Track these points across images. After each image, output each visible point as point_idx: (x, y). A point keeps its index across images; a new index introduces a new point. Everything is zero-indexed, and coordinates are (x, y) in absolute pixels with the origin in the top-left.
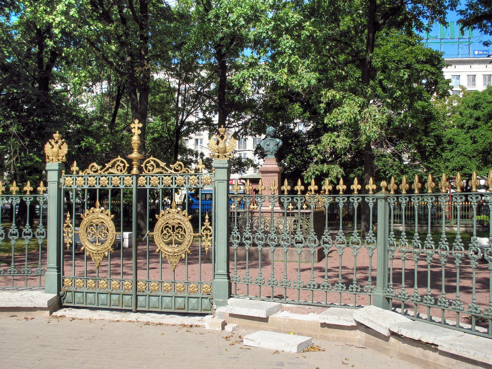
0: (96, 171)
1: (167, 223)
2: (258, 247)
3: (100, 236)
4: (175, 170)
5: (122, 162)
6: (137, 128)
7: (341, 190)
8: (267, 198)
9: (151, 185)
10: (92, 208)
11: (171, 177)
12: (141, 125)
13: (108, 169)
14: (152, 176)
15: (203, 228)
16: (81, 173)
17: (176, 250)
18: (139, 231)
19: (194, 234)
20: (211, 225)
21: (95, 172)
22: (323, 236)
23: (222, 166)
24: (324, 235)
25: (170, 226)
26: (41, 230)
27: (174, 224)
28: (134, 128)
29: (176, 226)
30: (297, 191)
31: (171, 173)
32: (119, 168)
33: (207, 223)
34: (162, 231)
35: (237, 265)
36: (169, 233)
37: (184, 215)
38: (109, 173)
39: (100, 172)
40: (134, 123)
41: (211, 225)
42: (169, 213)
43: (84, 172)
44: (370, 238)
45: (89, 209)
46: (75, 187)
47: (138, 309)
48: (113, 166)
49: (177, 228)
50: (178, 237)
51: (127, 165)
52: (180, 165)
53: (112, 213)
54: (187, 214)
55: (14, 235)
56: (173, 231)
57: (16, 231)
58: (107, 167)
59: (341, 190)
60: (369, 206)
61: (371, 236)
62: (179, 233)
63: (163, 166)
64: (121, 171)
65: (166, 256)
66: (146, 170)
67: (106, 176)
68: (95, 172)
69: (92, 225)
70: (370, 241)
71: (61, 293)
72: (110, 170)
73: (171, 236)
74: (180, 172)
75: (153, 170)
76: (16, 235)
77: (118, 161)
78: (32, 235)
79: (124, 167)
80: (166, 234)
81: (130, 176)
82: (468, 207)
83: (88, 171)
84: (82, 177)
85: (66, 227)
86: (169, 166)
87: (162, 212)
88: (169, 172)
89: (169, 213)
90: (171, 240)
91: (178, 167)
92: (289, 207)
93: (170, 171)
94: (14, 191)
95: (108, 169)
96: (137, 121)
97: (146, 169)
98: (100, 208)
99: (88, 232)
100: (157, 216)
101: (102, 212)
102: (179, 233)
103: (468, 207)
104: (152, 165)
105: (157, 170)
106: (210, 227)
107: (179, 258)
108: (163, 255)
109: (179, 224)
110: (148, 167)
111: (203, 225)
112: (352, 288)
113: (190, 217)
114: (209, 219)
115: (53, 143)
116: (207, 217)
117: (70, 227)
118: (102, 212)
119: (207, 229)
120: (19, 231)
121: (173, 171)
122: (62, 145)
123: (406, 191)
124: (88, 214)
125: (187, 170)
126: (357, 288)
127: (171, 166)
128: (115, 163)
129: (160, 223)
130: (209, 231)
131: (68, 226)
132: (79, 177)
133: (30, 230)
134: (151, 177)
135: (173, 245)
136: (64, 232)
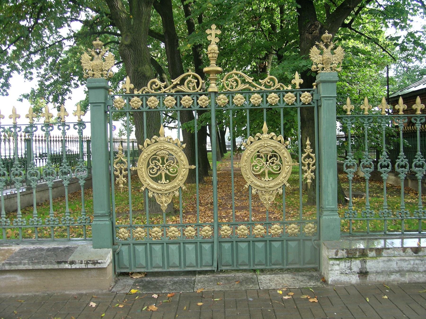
0: (160, 89)
1: (155, 154)
2: (348, 176)
3: (168, 172)
5: (196, 78)
6: (213, 35)
8: (72, 125)
10: (258, 134)
12: (219, 32)
16: (136, 92)
17: (168, 187)
20: (313, 152)
21: (156, 90)
24: (416, 158)
26: (402, 161)
27: (163, 155)
28: (211, 34)
30: (416, 110)
31: (261, 89)
32: (191, 85)
34: (148, 164)
36: (157, 166)
37: (280, 141)
39: (163, 90)
40: (211, 29)
43: (141, 90)
44: (17, 170)
45: (150, 137)
49: (270, 158)
50: (272, 169)
52: (272, 79)
55: (402, 167)
56: (163, 163)
57: (389, 161)
58: (175, 83)
61: (419, 158)
62: (273, 163)
63: (251, 81)
67: (172, 95)
72: (179, 88)
73: (159, 169)
74: (272, 88)
76: (387, 167)
77: (189, 76)
79: (198, 84)
80: (153, 168)
83: (148, 88)
85: (306, 157)
88: (258, 89)
89: (156, 142)
90: (264, 172)
95: (175, 87)
96: (214, 27)
98: (269, 133)
99: (150, 166)
101: (272, 138)
102: (169, 166)
107: (275, 193)
108: (254, 192)
109: (273, 151)
111: (303, 152)
115: (322, 46)
116: (308, 142)
118: (272, 138)
121: (263, 88)
124: (148, 145)
127: (260, 81)
131: (309, 157)
135: (267, 178)
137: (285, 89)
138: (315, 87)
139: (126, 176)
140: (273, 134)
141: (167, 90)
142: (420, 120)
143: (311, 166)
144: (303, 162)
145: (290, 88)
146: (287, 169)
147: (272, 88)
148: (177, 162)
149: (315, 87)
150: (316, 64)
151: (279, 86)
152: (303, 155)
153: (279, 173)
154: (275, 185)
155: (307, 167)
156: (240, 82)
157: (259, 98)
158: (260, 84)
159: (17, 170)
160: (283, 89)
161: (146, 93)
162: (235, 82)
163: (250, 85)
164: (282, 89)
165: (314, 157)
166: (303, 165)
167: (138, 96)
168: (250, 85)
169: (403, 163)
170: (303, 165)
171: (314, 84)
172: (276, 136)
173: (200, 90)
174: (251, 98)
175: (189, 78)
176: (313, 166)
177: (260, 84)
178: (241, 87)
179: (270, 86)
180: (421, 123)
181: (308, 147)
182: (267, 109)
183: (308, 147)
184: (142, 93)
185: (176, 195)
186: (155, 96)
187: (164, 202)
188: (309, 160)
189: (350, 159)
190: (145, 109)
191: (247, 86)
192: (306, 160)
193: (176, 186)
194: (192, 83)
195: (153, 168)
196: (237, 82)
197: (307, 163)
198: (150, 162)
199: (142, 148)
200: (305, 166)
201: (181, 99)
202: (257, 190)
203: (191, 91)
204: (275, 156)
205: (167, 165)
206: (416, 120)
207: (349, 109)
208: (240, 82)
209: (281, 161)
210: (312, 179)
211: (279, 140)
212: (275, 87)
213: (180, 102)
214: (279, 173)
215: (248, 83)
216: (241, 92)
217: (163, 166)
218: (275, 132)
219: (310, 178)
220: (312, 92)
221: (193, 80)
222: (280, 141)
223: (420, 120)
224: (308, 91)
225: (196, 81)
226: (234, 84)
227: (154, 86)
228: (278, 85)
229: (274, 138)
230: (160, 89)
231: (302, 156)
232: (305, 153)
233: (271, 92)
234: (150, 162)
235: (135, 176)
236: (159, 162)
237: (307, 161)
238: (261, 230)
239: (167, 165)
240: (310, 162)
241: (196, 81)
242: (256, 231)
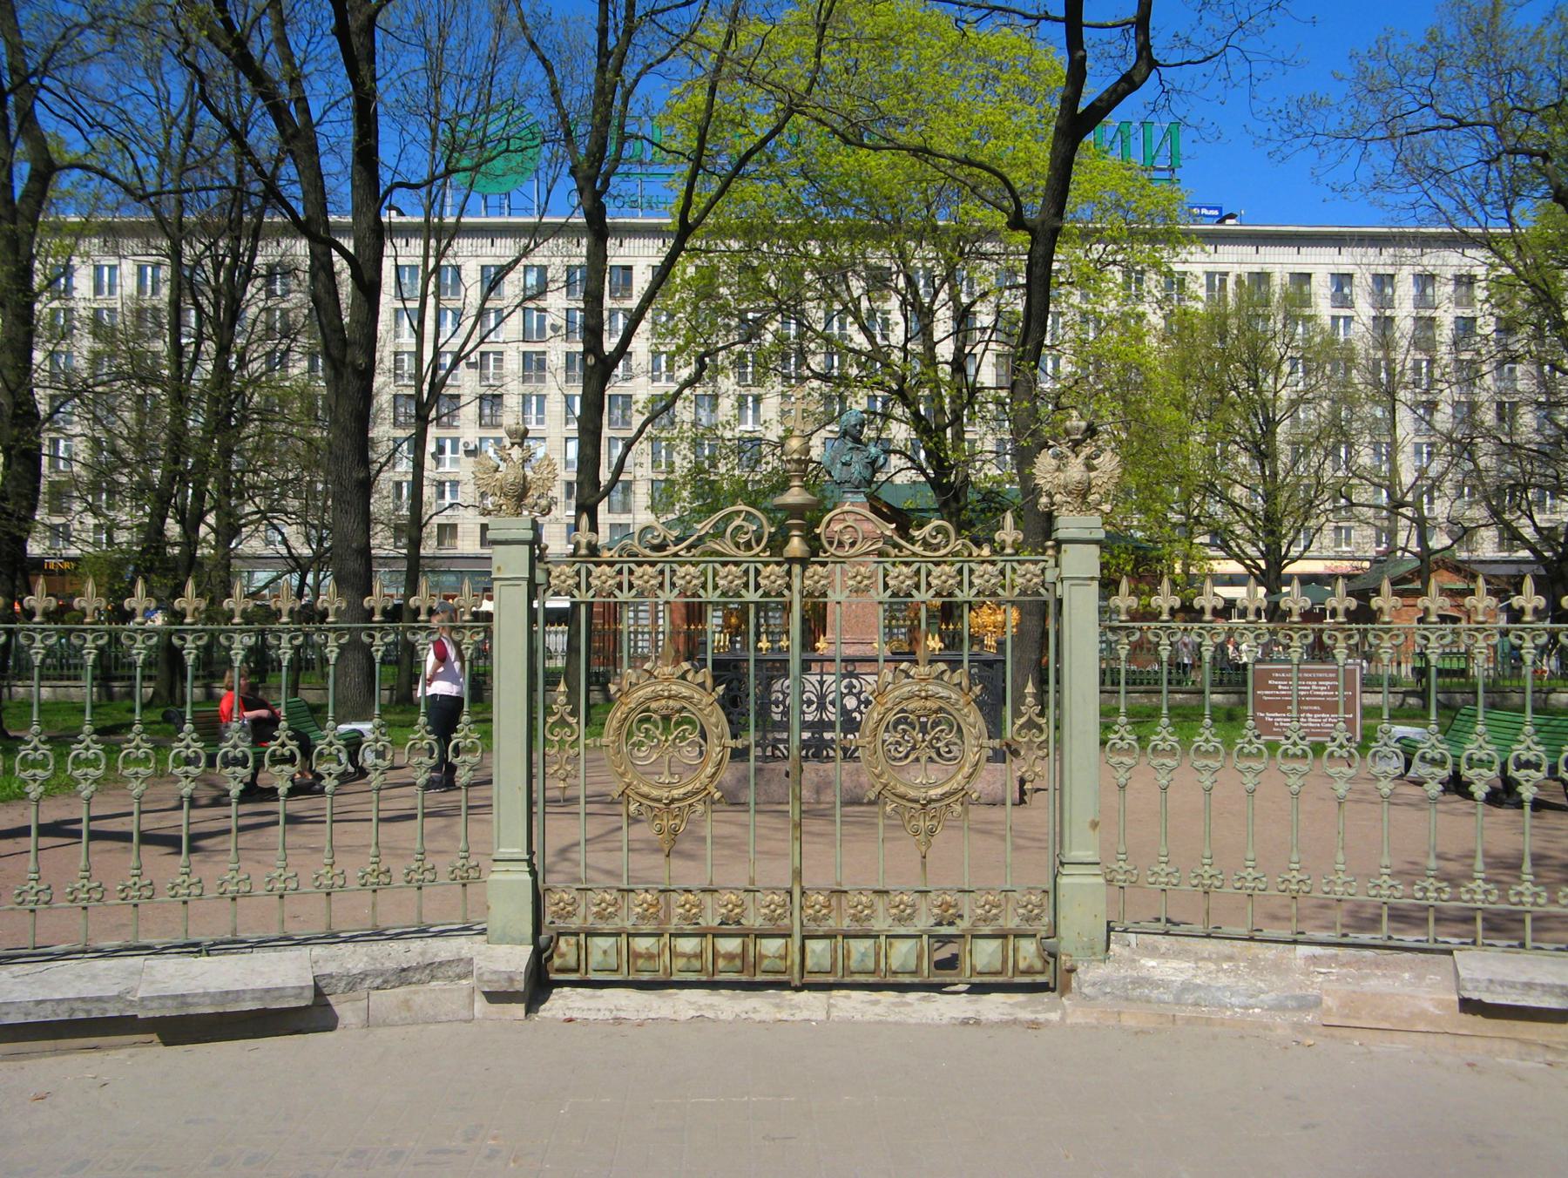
4: (926, 544)
9: (761, 592)
11: (915, 566)
14: (937, 564)
19: (732, 743)
22: (1154, 737)
23: (1086, 535)
31: (914, 554)
33: (1030, 706)
35: (238, 816)
37: (702, 685)
38: (703, 554)
46: (588, 597)
47: (809, 979)
48: (718, 533)
49: (678, 724)
51: (770, 529)
54: (709, 682)
59: (285, 612)
60: (182, 658)
62: (684, 739)
65: (643, 809)
69: (648, 719)
70: (1162, 746)
71: (543, 938)
74: (943, 552)
78: (1544, 768)
80: (641, 744)
81: (779, 564)
82: (170, 657)
84: (611, 564)
86: (907, 533)
94: (1166, 607)
103: (170, 657)
112: (1520, 894)
113: (721, 689)
114: (1035, 696)
116: (1030, 689)
117: (569, 725)
118: (683, 677)
119: (1030, 725)
120: (299, 747)
121: (918, 549)
123: (1301, 615)
126: (1535, 895)
128: (728, 518)
132: (598, 564)
133: (1443, 748)
134: (931, 566)
140: (686, 666)
142: (292, 638)
147: (943, 552)
148: (960, 729)
150: (1050, 495)
154: (686, 796)
159: (1122, 739)
169: (141, 754)
173: (764, 550)
175: (738, 522)
177: (912, 541)
180: (1536, 647)
181: (1029, 700)
182: (756, 603)
183: (1029, 700)
189: (1164, 733)
206: (1520, 638)
207: (190, 609)
211: (956, 681)
220: (1041, 565)
222: (702, 685)
223: (292, 638)
228: (956, 544)
229: (689, 677)
232: (1022, 715)
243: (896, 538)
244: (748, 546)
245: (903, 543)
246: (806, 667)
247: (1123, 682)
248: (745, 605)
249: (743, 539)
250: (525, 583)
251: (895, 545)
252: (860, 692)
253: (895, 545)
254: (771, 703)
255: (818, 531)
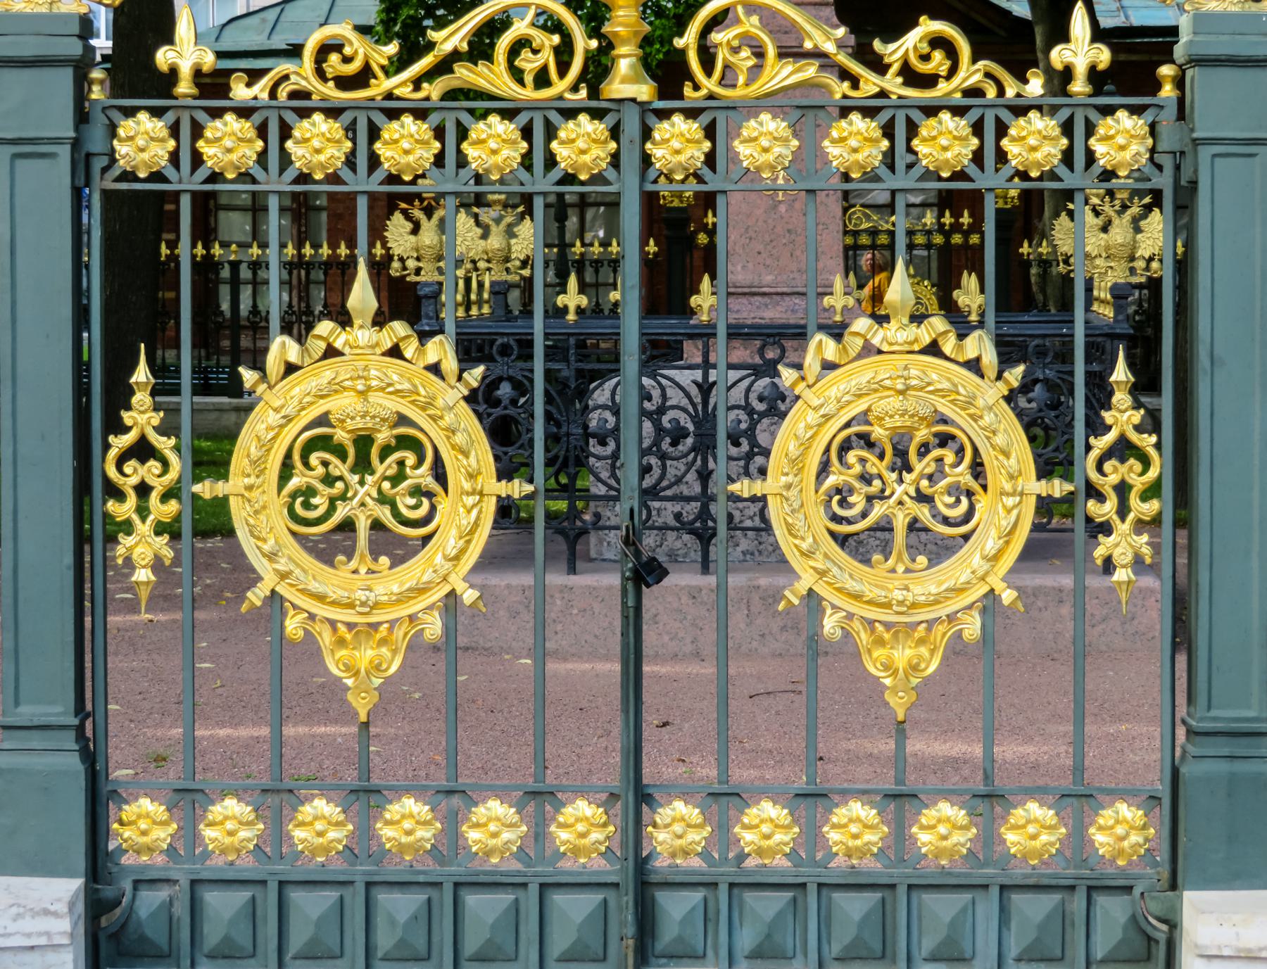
0: (363, 78)
3: (385, 514)
4: (911, 76)
7: (572, 309)
10: (325, 327)
13: (444, 67)
15: (1102, 443)
18: (440, 471)
21: (344, 83)
25: (341, 436)
29: (383, 436)
31: (883, 94)
32: (529, 63)
34: (286, 470)
37: (435, 369)
41: (1152, 423)
42: (331, 352)
48: (480, 49)
53: (1008, 352)
58: (448, 47)
59: (572, 309)
63: (830, 47)
64: (542, 79)
66: (709, 72)
68: (344, 83)
72: (464, 74)
74: (943, 87)
75: (756, 70)
87: (282, 348)
89: (331, 352)
91: (926, 58)
92: (561, 300)
93: (871, 83)
95: (444, 67)
97: (708, 61)
100: (248, 376)
104: (748, 40)
105: (780, 74)
106: (1147, 441)
109: (403, 420)
110: (722, 56)
111: (1096, 427)
121: (893, 83)
122: (1144, 216)
125: (988, 75)
129: (273, 418)
130: (1138, 467)
136: (115, 492)
137: (1010, 93)
138: (1168, 91)
139: (169, 529)
140: (399, 328)
141: (403, 84)
143: (154, 497)
144: (1094, 476)
145: (1035, 86)
146: (1009, 511)
149: (1168, 91)
151: (978, 77)
152: (111, 438)
153: (966, 537)
154: (402, 599)
155: (1111, 505)
156: (771, 51)
157: (873, 141)
158: (879, 67)
160: (1001, 92)
161: (294, 95)
162: (746, 52)
163: (822, 67)
164: (991, 93)
165: (1153, 453)
166: (1093, 492)
167: (244, 112)
168: (822, 67)
170: (1093, 492)
171: (1166, 70)
172: (414, 343)
173: (575, 88)
174: (916, 135)
176: (165, 497)
177: (879, 67)
178: (780, 74)
179: (929, 81)
181: (1121, 398)
182: (372, 197)
184: (273, 94)
185: (966, 635)
186: (333, 112)
187: (362, 669)
188: (1123, 469)
190: (187, 182)
191: (810, 70)
192: (127, 469)
193: (421, 590)
194: (535, 52)
195: (309, 492)
196: (760, 54)
197: (134, 480)
198: (296, 457)
199: (255, 384)
200: (1101, 498)
201: (463, 133)
202: (850, 616)
203: (528, 93)
204: (944, 440)
205: (386, 478)
208: (771, 51)
209: (978, 469)
210: (157, 565)
212: (956, 81)
213: (459, 151)
214: (966, 537)
215: (818, 54)
216: (773, 102)
217: (901, 481)
218: (413, 320)
219: (1129, 558)
221: (539, 37)
224: (1136, 110)
225: (556, 39)
226: (745, 59)
227: (334, 58)
228: (971, 73)
230: (363, 78)
231: (1088, 448)
232: (127, 430)
233: (931, 111)
234: (296, 457)
235: (213, 523)
236: (343, 458)
237: (1115, 472)
238: (955, 827)
239: (386, 478)
240: (150, 481)
241: (556, 39)
242: (564, 835)
243: (843, 59)
244: (542, 79)
245: (856, 68)
246: (661, 352)
247: (274, 274)
248: (351, 197)
249: (529, 63)
250: (65, 152)
251: (845, 75)
252: (750, 411)
253: (845, 75)
254: (587, 435)
255: (679, 43)
